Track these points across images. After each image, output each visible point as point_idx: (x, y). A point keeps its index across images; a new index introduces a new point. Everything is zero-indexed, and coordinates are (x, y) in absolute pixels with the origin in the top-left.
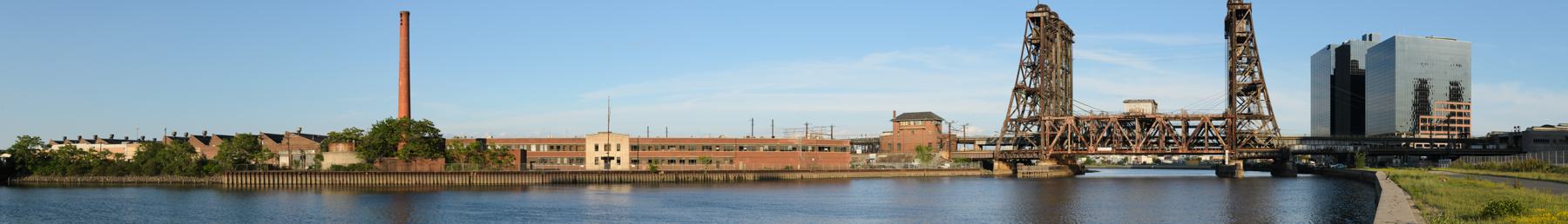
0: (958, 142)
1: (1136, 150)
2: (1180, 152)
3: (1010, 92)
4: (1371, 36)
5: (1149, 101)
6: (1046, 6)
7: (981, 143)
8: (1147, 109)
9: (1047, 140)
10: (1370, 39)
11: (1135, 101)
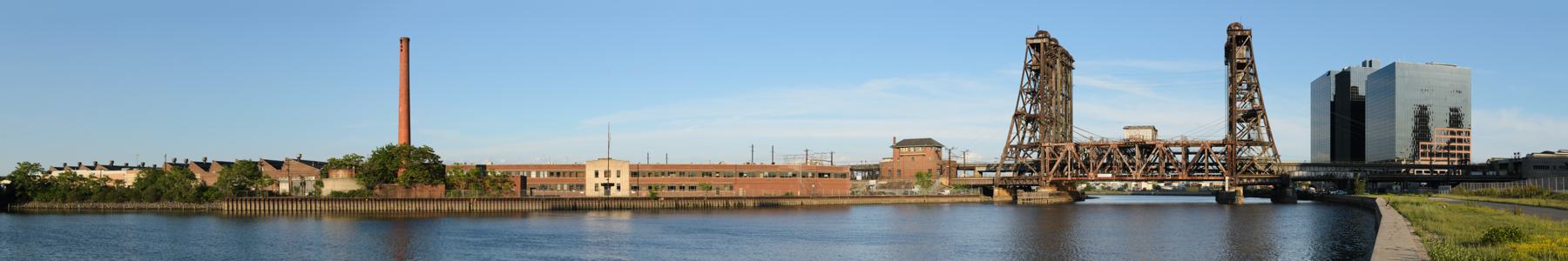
0: (958, 168)
2: (1180, 178)
3: (1010, 118)
4: (1371, 62)
5: (1149, 127)
6: (1046, 32)
7: (981, 169)
8: (1147, 136)
9: (1047, 166)
10: (1370, 66)
11: (1135, 128)
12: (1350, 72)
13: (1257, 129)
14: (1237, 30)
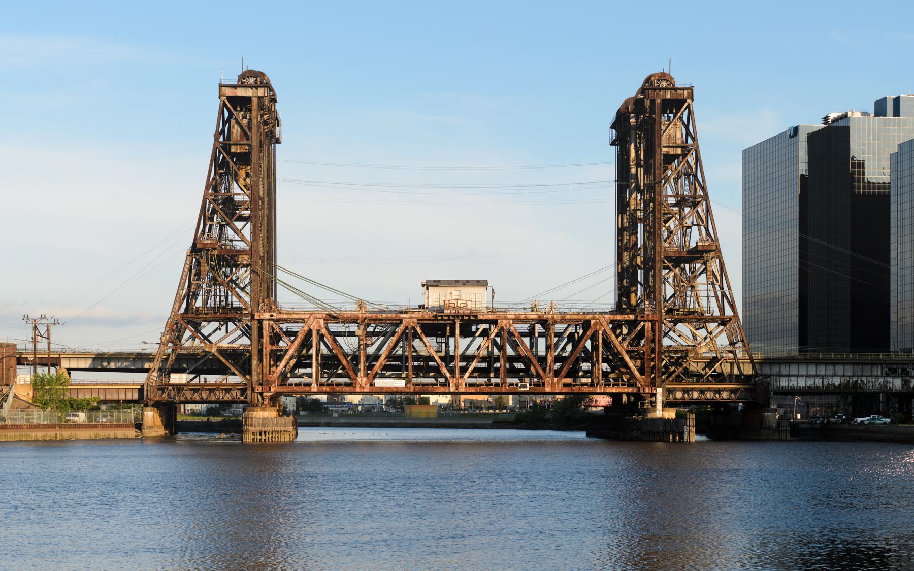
0: (20, 362)
1: (457, 386)
4: (897, 101)
6: (261, 74)
10: (897, 113)
12: (846, 131)
13: (233, 195)
14: (666, 89)
